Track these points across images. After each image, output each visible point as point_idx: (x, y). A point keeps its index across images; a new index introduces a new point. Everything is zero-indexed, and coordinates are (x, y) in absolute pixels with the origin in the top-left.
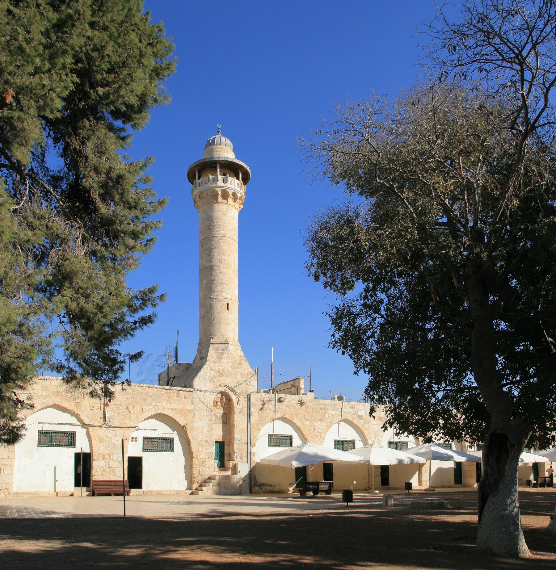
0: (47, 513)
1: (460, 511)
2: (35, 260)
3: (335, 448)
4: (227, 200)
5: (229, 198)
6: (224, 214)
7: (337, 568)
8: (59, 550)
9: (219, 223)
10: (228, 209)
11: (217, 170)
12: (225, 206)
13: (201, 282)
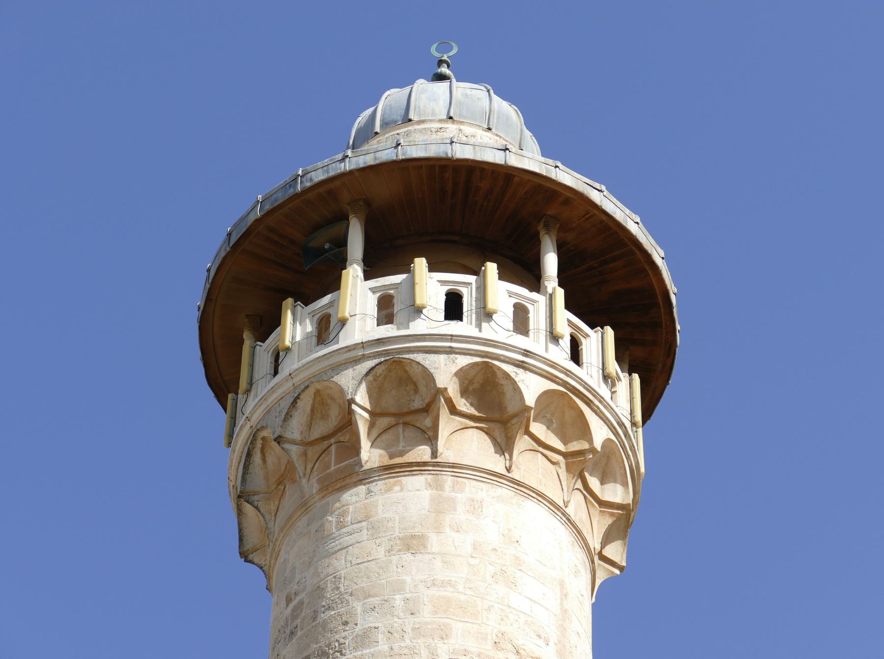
0: (242, 219)
1: (426, 468)
2: (344, 512)
3: (500, 278)
4: (430, 437)
5: (447, 424)
6: (413, 543)
7: (643, 470)
8: (322, 537)
9: (364, 622)
10: (440, 507)
11: (383, 116)
12: (416, 482)
13: (410, 450)
